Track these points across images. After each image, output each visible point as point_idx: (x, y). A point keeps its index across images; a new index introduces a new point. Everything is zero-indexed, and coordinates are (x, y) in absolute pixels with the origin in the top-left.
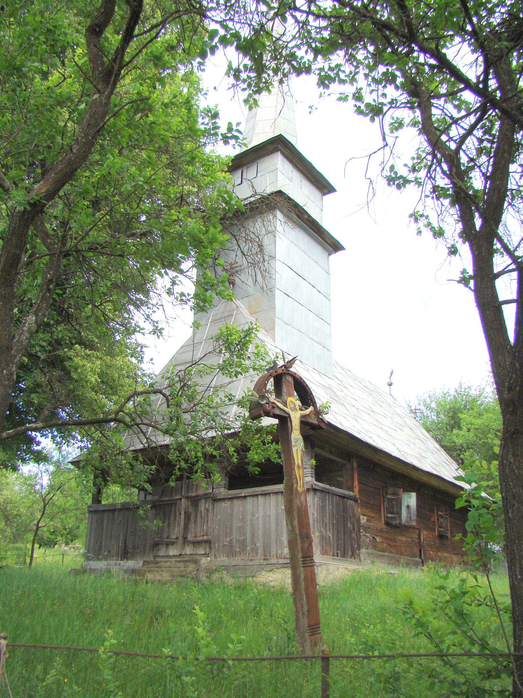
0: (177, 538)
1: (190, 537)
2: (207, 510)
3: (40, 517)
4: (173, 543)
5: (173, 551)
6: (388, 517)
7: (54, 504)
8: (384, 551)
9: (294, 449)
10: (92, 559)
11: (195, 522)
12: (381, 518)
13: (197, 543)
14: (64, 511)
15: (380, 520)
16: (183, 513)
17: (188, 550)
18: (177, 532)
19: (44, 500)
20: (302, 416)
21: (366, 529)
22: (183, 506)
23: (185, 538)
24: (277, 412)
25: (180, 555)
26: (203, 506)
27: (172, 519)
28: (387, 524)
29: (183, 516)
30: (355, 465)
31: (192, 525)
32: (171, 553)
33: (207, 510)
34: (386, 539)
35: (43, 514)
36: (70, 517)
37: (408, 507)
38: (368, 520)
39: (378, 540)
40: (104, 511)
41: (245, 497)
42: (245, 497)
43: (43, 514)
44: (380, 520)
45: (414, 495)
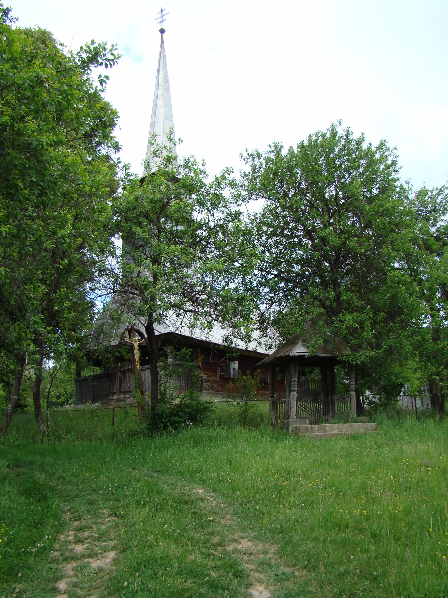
0: (117, 391)
1: (122, 390)
2: (129, 376)
3: (49, 387)
4: (115, 393)
5: (115, 397)
6: (221, 375)
7: (57, 378)
8: (219, 391)
9: (136, 356)
10: (79, 404)
11: (124, 382)
12: (216, 375)
13: (125, 392)
14: (64, 382)
15: (216, 376)
16: (119, 378)
17: (122, 396)
18: (116, 388)
19: (51, 376)
20: (139, 344)
21: (207, 381)
22: (119, 375)
23: (120, 390)
24: (128, 344)
25: (119, 398)
26: (127, 374)
27: (114, 382)
28: (220, 378)
29: (119, 380)
30: (199, 351)
31: (123, 384)
32: (114, 398)
33: (129, 376)
34: (221, 385)
35: (52, 384)
36: (68, 385)
37: (234, 369)
38: (208, 377)
39: (215, 386)
40: (82, 380)
41: (145, 369)
42: (145, 369)
43: (52, 384)
44: (216, 376)
45: (237, 363)
